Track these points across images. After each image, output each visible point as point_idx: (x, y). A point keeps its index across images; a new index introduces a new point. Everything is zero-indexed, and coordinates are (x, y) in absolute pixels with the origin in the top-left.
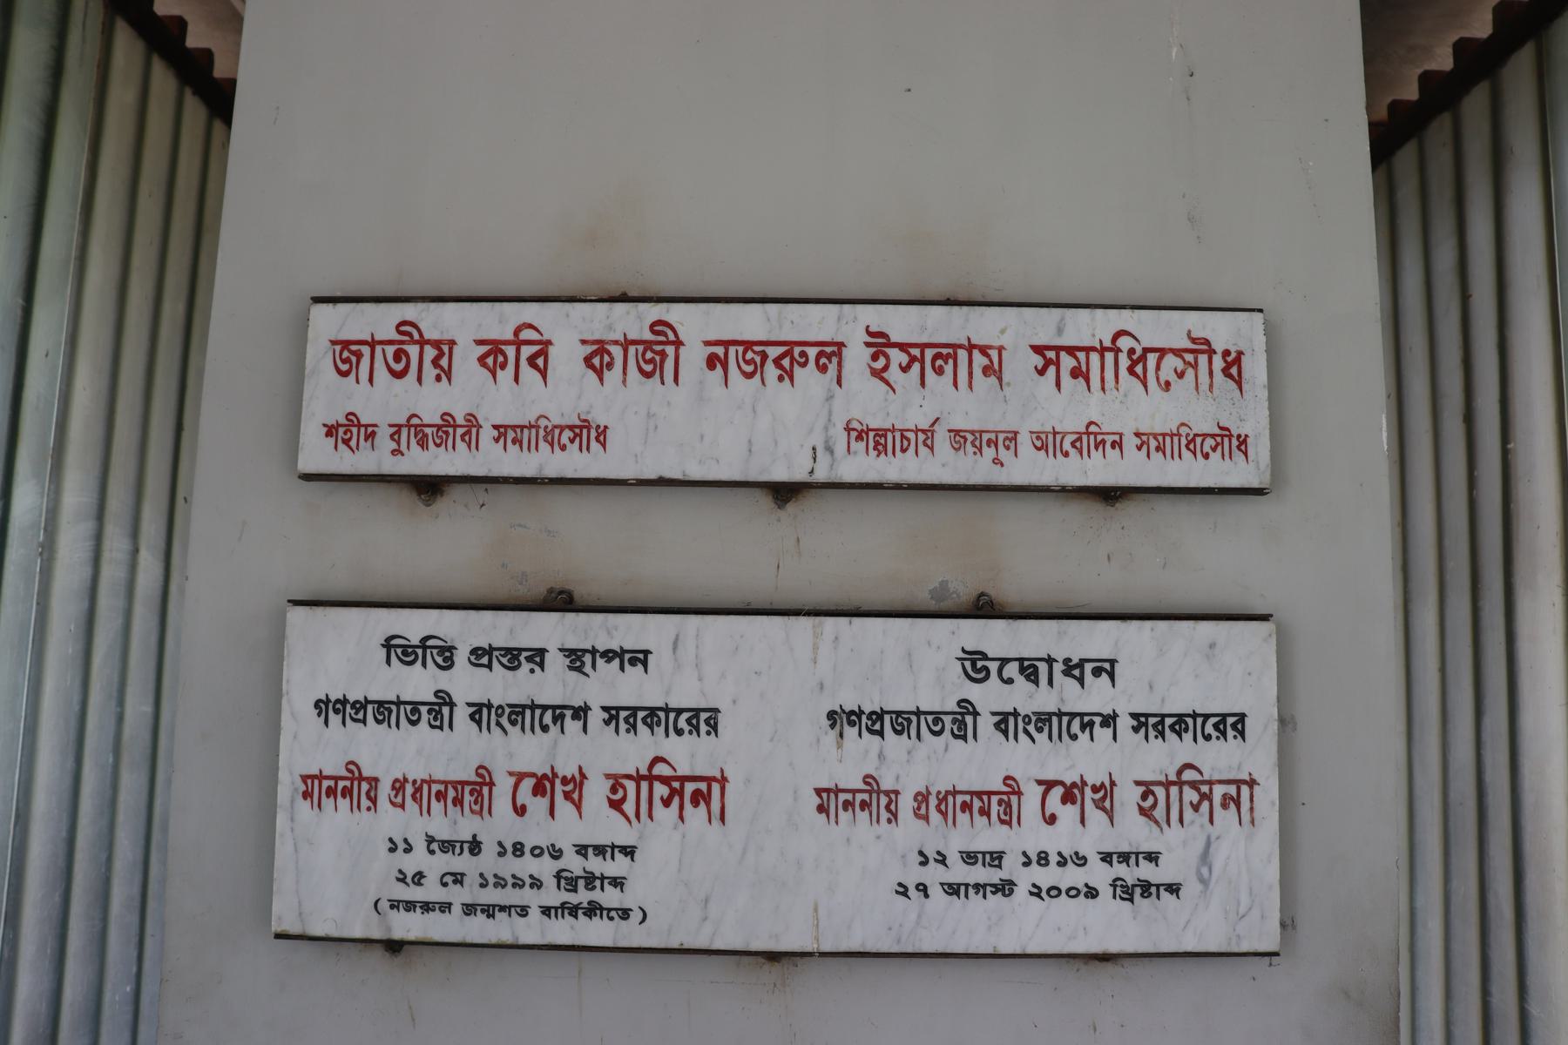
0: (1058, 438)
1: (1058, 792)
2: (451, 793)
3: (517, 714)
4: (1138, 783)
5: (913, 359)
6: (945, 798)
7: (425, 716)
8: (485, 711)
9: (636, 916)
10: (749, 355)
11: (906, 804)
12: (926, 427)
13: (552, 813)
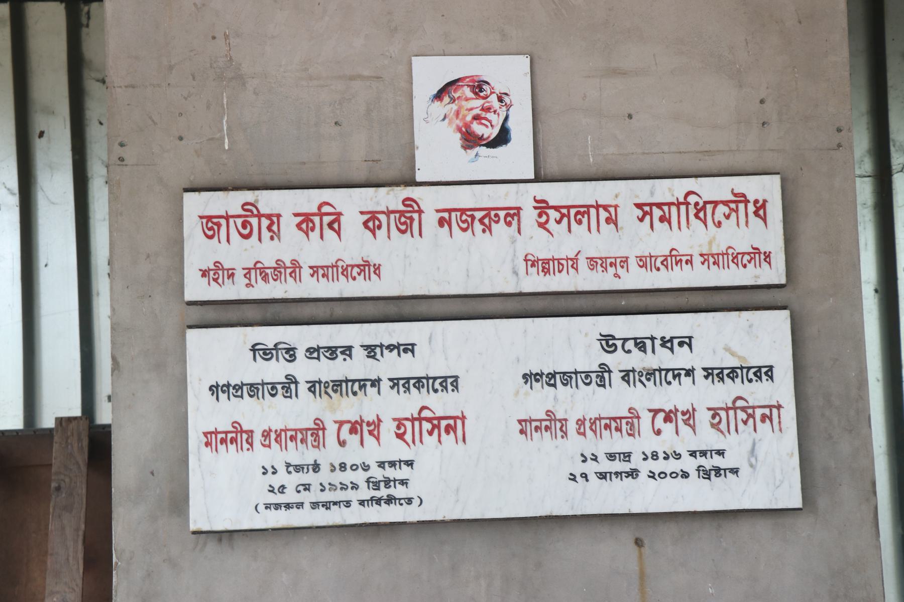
0: (653, 259)
1: (661, 416)
2: (299, 436)
3: (337, 386)
4: (709, 409)
5: (563, 216)
6: (595, 422)
8: (317, 385)
9: (416, 502)
10: (464, 217)
11: (572, 427)
12: (573, 257)
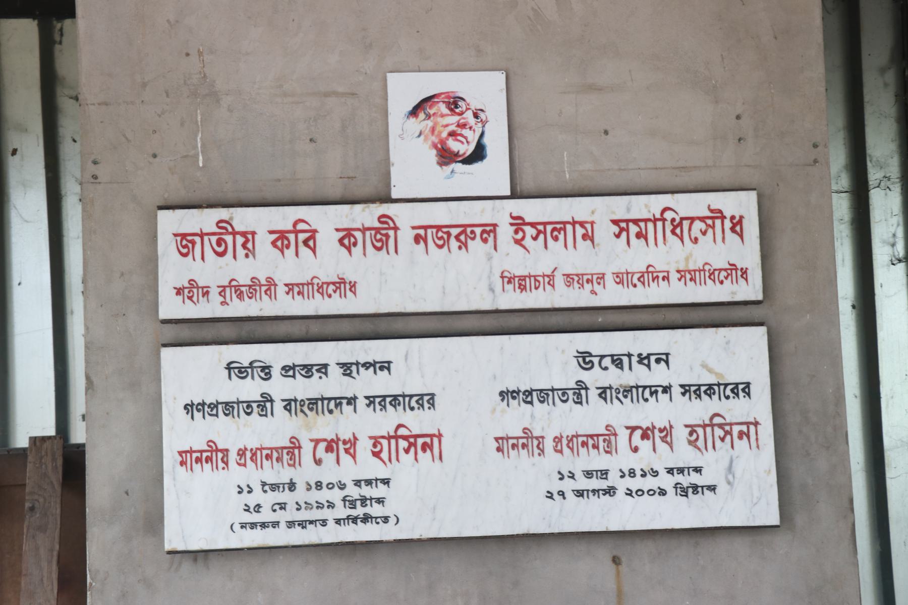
0: (630, 276)
1: (638, 433)
2: (275, 455)
3: (313, 404)
4: (686, 426)
5: (539, 232)
6: (572, 440)
10: (440, 234)
11: (549, 444)
12: (549, 273)
13: (338, 462)
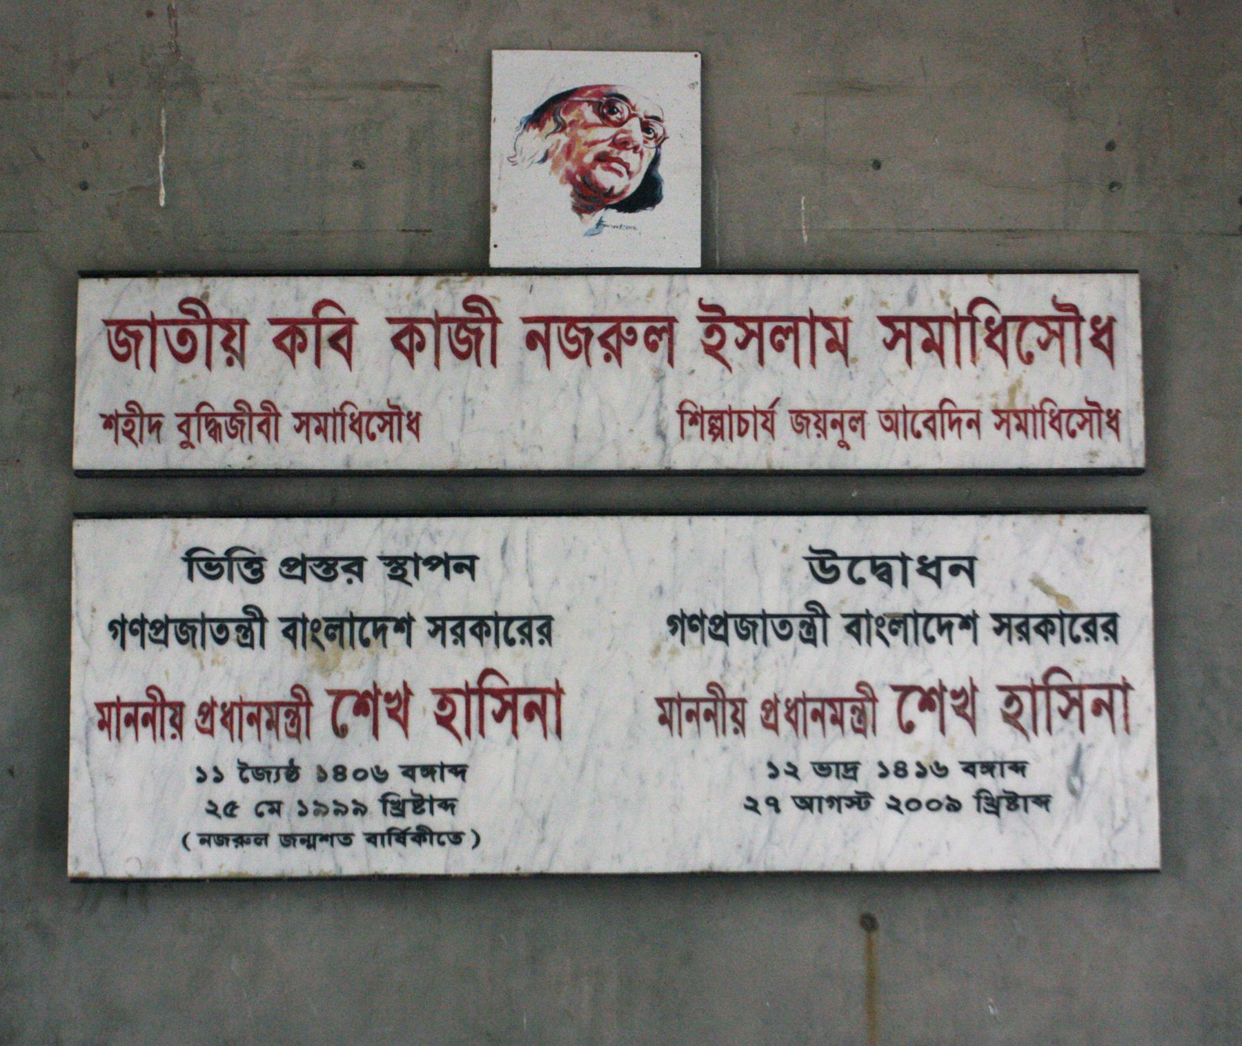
1: (915, 698)
2: (265, 716)
3: (335, 627)
5: (750, 335)
6: (795, 707)
7: (233, 634)
9: (469, 839)
10: (573, 333)
11: (753, 713)
